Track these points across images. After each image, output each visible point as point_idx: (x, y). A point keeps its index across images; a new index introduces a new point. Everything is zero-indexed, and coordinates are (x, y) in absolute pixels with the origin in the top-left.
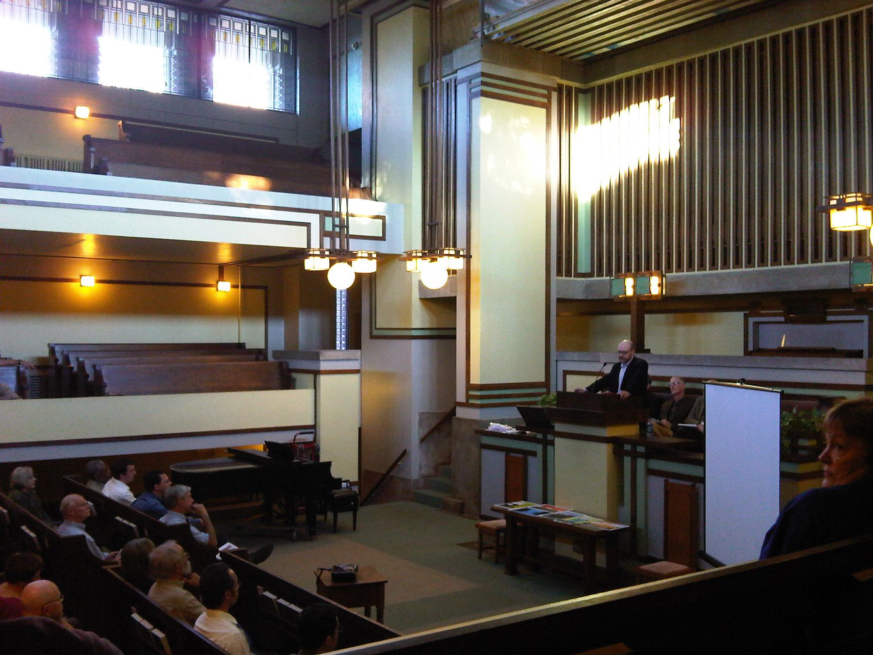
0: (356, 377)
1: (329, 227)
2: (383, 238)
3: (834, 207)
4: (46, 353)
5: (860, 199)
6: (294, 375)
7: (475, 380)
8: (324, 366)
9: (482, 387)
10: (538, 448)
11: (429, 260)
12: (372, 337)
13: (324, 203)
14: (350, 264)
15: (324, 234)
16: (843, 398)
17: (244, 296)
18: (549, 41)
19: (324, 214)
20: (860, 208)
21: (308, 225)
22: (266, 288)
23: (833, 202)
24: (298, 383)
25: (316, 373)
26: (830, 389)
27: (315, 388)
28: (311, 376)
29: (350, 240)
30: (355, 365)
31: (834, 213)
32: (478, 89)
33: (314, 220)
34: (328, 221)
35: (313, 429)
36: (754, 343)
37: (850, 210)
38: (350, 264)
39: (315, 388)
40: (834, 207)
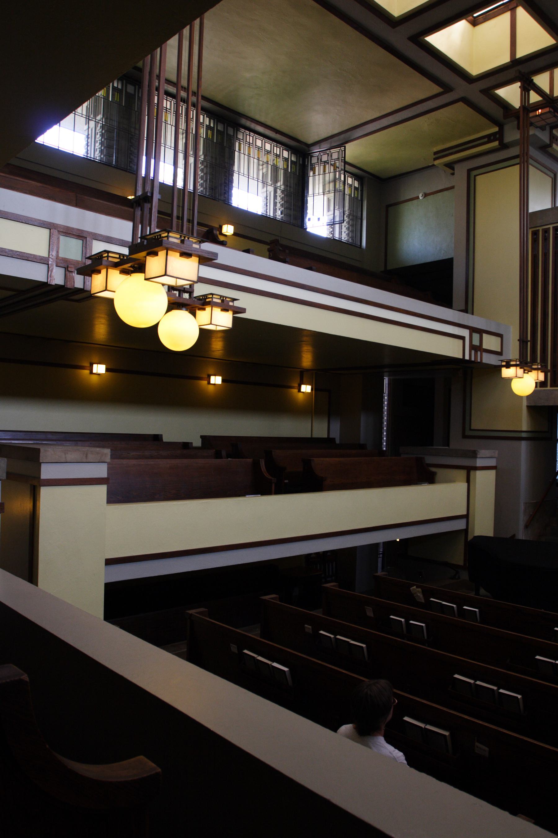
0: (493, 473)
8: (479, 463)
15: (472, 347)
19: (473, 330)
20: (518, 368)
21: (463, 338)
24: (437, 477)
25: (470, 470)
27: (468, 481)
28: (463, 473)
30: (493, 463)
35: (466, 517)
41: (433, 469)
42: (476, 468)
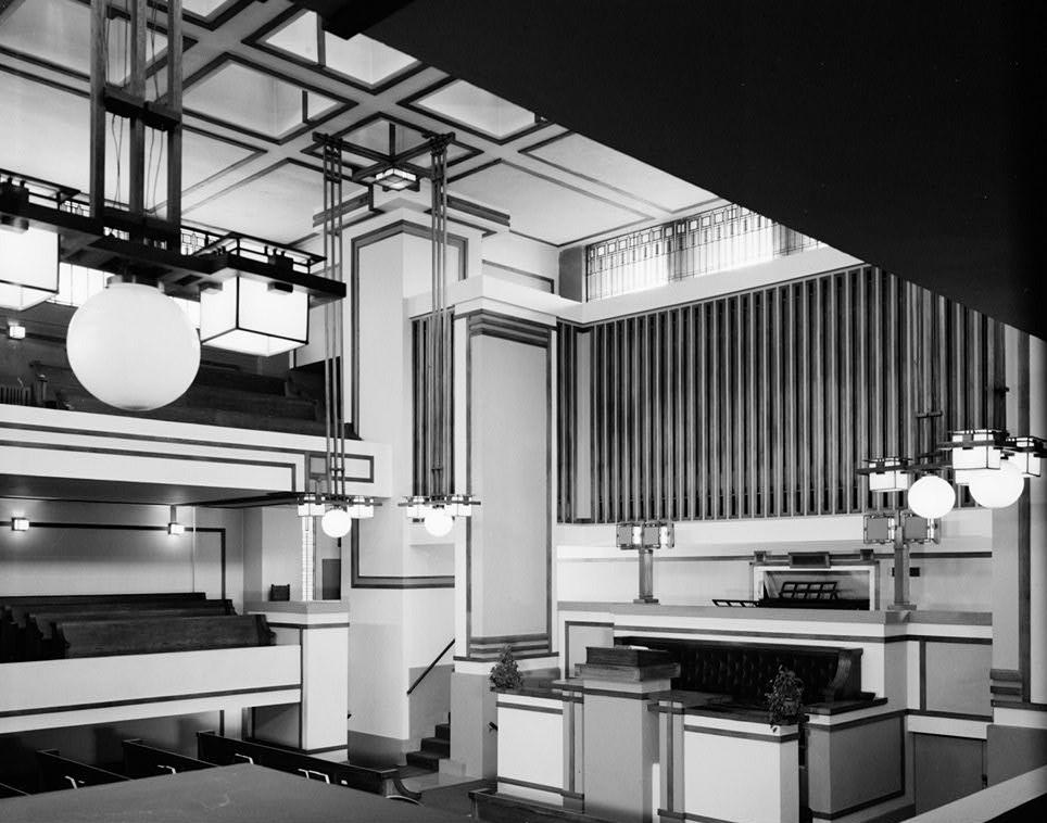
1: (315, 469)
2: (371, 480)
3: (873, 470)
4: (654, 598)
5: (898, 464)
6: (273, 629)
7: (477, 633)
9: (483, 641)
10: (872, 568)
11: (431, 506)
12: (354, 586)
13: (317, 443)
14: (345, 509)
15: (311, 476)
16: (200, 278)
17: (199, 541)
18: (704, 469)
21: (292, 466)
22: (222, 531)
23: (873, 466)
26: (1010, 702)
27: (301, 644)
29: (346, 483)
31: (873, 476)
32: (479, 326)
33: (299, 460)
34: (315, 461)
36: (650, 776)
37: (889, 474)
38: (345, 509)
39: (301, 644)
40: (873, 470)
41: (273, 629)
42: (306, 627)
